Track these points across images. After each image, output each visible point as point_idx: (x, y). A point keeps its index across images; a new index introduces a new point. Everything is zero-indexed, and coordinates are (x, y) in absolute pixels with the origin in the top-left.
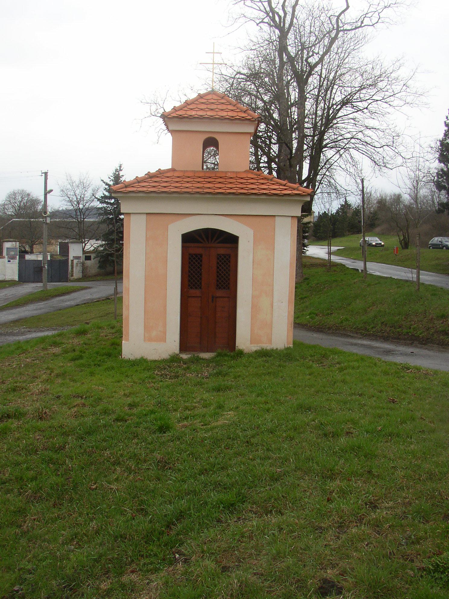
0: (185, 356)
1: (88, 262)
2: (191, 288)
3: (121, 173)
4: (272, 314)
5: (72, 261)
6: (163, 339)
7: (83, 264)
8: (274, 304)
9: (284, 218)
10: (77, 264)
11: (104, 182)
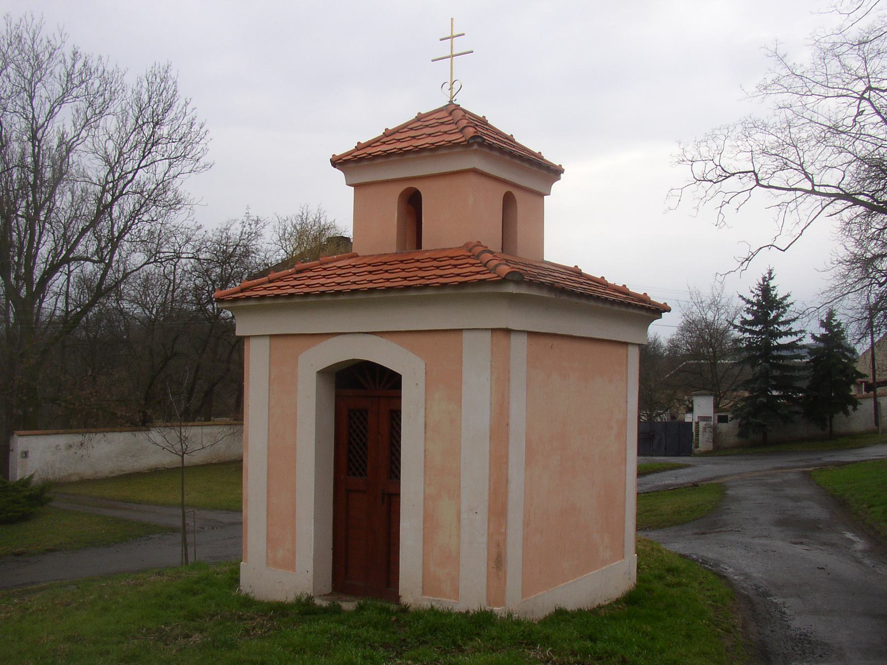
0: (348, 605)
1: (723, 427)
3: (772, 283)
4: (459, 536)
5: (697, 423)
6: (290, 565)
7: (714, 429)
8: (464, 516)
10: (705, 428)
11: (744, 299)
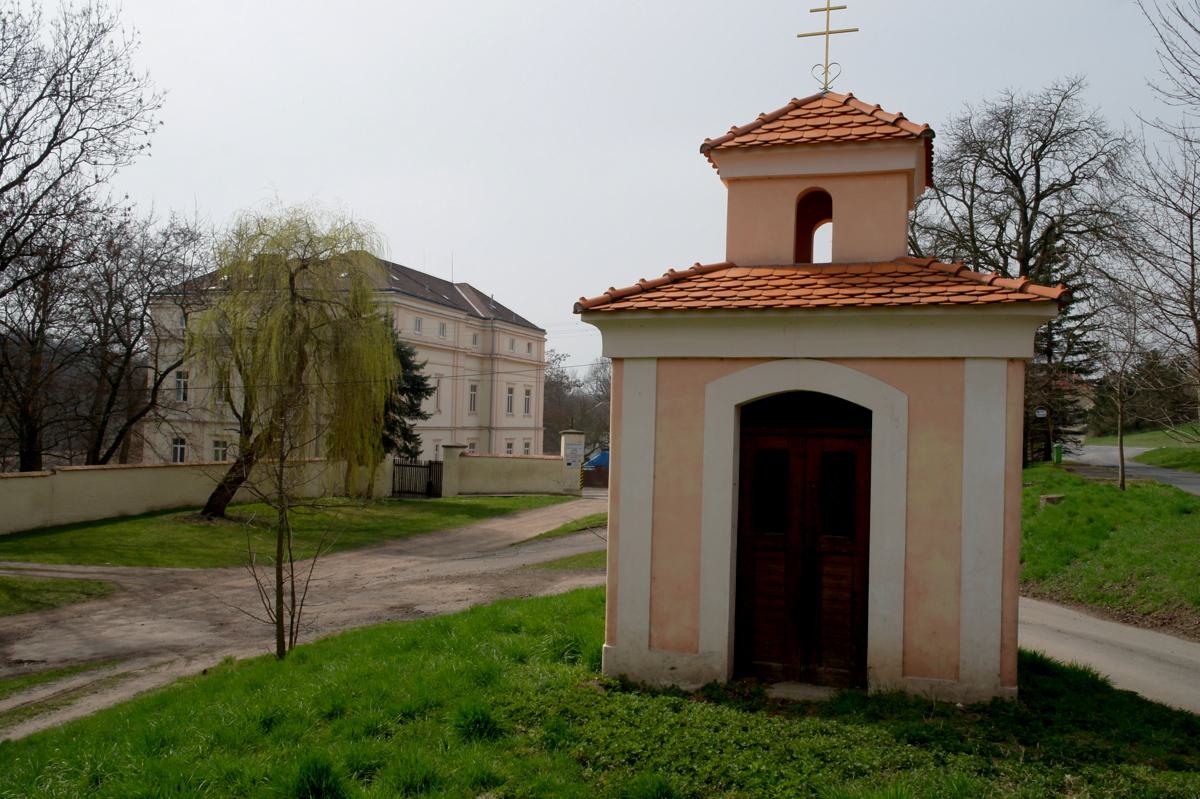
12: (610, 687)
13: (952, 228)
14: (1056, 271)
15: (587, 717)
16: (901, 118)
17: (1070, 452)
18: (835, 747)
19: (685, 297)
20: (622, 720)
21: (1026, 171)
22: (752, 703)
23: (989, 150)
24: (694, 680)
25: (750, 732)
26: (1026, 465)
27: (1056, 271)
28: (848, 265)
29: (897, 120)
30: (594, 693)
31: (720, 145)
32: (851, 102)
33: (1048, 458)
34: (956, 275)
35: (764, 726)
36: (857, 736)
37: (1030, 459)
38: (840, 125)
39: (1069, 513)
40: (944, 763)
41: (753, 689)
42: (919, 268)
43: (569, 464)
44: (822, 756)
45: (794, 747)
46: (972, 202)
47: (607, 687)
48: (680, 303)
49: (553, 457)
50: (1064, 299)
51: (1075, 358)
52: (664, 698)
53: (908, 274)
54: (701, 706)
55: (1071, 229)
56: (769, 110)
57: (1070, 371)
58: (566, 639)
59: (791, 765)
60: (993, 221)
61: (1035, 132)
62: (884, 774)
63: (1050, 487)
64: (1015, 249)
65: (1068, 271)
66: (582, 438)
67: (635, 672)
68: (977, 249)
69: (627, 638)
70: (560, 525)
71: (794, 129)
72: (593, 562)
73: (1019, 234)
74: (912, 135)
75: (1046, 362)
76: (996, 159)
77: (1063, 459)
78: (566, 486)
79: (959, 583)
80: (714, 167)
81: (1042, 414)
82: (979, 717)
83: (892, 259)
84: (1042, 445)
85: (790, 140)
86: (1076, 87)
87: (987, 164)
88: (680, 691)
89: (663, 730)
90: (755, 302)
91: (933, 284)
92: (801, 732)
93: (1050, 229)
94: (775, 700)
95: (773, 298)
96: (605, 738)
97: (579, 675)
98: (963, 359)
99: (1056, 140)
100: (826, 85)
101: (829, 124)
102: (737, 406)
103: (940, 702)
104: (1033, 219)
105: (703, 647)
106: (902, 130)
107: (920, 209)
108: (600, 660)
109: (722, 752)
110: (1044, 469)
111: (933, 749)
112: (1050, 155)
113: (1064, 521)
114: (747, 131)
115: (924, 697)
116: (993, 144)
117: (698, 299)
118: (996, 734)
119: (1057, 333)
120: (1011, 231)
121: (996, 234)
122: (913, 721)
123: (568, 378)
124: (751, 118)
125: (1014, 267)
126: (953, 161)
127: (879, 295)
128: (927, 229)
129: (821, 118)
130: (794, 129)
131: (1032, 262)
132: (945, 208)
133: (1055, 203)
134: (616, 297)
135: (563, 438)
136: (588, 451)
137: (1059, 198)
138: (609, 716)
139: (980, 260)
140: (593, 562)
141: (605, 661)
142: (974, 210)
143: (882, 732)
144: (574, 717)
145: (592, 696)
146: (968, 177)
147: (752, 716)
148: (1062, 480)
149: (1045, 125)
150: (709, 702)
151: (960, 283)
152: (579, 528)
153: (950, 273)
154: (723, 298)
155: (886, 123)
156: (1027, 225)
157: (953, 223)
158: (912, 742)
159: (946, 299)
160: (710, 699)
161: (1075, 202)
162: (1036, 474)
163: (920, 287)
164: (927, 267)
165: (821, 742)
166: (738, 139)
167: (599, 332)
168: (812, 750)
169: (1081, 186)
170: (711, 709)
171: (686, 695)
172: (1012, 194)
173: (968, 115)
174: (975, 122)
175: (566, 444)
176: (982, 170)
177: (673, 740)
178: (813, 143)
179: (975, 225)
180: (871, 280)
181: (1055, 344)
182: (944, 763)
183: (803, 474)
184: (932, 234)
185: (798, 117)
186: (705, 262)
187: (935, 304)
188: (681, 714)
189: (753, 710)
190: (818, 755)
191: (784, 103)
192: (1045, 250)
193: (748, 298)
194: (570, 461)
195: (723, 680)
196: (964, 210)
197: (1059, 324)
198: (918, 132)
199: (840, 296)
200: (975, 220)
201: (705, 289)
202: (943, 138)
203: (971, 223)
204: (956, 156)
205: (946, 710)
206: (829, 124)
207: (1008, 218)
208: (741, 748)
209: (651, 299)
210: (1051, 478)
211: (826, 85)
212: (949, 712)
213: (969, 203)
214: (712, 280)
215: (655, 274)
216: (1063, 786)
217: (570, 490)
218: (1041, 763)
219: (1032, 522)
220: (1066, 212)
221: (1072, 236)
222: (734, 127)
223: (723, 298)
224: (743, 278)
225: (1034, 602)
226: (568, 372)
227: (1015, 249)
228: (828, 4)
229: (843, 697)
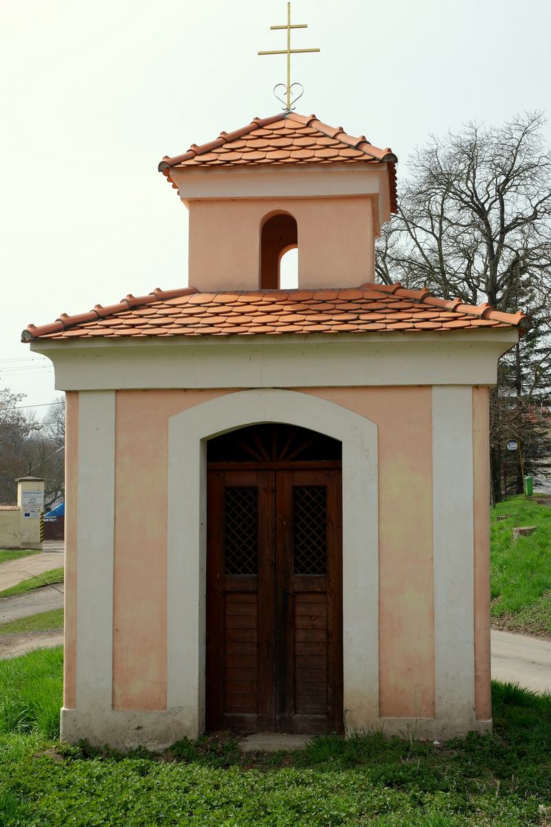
2: (234, 571)
9: (454, 390)
12: (70, 755)
13: (422, 260)
14: (523, 304)
15: (42, 791)
16: (364, 142)
17: (541, 484)
18: (311, 797)
19: (147, 323)
20: (82, 789)
21: (491, 204)
22: (223, 759)
23: (455, 183)
24: (162, 738)
25: (221, 789)
26: (497, 496)
27: (523, 304)
28: (314, 291)
29: (360, 143)
30: (51, 763)
31: (180, 163)
32: (314, 124)
33: (520, 491)
34: (421, 301)
35: (235, 781)
36: (334, 784)
37: (503, 492)
38: (304, 147)
39: (540, 544)
40: (421, 804)
41: (226, 743)
42: (390, 297)
43: (27, 515)
44: (297, 808)
45: (269, 801)
46: (441, 234)
47: (66, 755)
48: (139, 331)
49: (8, 507)
50: (523, 325)
51: (542, 391)
52: (129, 761)
53: (375, 301)
54: (169, 766)
55: (535, 262)
56: (231, 129)
57: (538, 403)
58: (19, 706)
59: (265, 820)
60: (461, 254)
61: (498, 166)
62: (362, 820)
63: (523, 520)
64: (483, 282)
65: (533, 305)
66: (41, 486)
67: (97, 734)
68: (446, 282)
69: (89, 697)
70: (17, 583)
71: (256, 149)
72: (50, 622)
73: (486, 267)
74: (375, 159)
75: (515, 395)
76: (462, 192)
77: (534, 491)
78: (24, 540)
79: (432, 615)
80: (174, 186)
81: (513, 446)
82: (456, 753)
83: (358, 286)
84: (514, 478)
85: (253, 161)
86: (536, 123)
87: (454, 196)
88: (147, 752)
89: (127, 796)
90: (219, 330)
91: (399, 310)
92: (276, 784)
93: (515, 263)
94: (250, 753)
95: (238, 325)
96: (62, 812)
97: (33, 745)
98: (430, 386)
99: (518, 175)
100: (289, 105)
101: (292, 145)
102: (201, 440)
103: (418, 741)
104: (499, 253)
105: (171, 703)
106: (364, 154)
107: (390, 241)
108: (58, 726)
109: (191, 814)
110: (518, 501)
111: (410, 790)
112: (513, 189)
113: (536, 553)
114: (208, 150)
115: (401, 737)
116: (458, 176)
117: (159, 326)
118: (473, 770)
119: (526, 366)
120: (479, 265)
121: (464, 266)
122: (390, 763)
123: (24, 421)
124: (211, 137)
125: (483, 299)
126: (421, 193)
127: (346, 322)
128: (399, 261)
129: (283, 139)
130: (256, 149)
131: (499, 295)
132: (415, 240)
133: (519, 236)
134: (69, 324)
135: (20, 486)
136: (49, 500)
137: (523, 232)
138: (67, 787)
139: (450, 293)
140: (50, 622)
141: (64, 726)
142: (443, 243)
143: (358, 776)
144: (27, 792)
145: (49, 766)
146: (436, 209)
147: (225, 772)
148: (533, 512)
149: (508, 159)
150: (178, 761)
151: (426, 310)
152: (38, 584)
153: (415, 300)
154: (185, 326)
155: (349, 147)
156: (493, 258)
157: (423, 255)
158: (390, 785)
159: (411, 325)
160: (179, 758)
161: (537, 236)
162: (509, 507)
163: (386, 313)
164: (393, 293)
165: (296, 793)
166: (197, 158)
167: (53, 369)
168: (287, 803)
169: (543, 220)
170: (181, 768)
171: (155, 756)
172: (478, 227)
173: (435, 147)
174: (441, 154)
175: (23, 493)
176: (450, 203)
177: (138, 806)
178: (276, 164)
179: (445, 258)
180: (339, 307)
181: (523, 377)
182: (421, 804)
183: (272, 508)
184: (403, 267)
185: (260, 137)
186: (166, 288)
187: (401, 330)
188: (148, 778)
189: (226, 766)
190: (293, 807)
191: (246, 123)
192: (511, 284)
193: (212, 325)
194: (28, 512)
195: (193, 736)
196: (433, 242)
197: (526, 357)
198: (381, 157)
199: (306, 323)
200: (444, 252)
201: (166, 315)
202: (411, 170)
203: (441, 255)
204: (424, 188)
205: (423, 749)
206: (292, 145)
207: (475, 251)
208: (213, 808)
209: (107, 327)
210: (522, 510)
211: (289, 105)
212: (426, 751)
213: (438, 235)
214: (174, 306)
215: (112, 300)
216: (537, 817)
217: (29, 544)
218: (516, 796)
219: (506, 555)
220: (530, 246)
221: (535, 269)
222: (194, 146)
223: (185, 326)
224: (207, 305)
225: (505, 635)
226: (25, 414)
227: (483, 282)
228: (289, 22)
229: (320, 744)
